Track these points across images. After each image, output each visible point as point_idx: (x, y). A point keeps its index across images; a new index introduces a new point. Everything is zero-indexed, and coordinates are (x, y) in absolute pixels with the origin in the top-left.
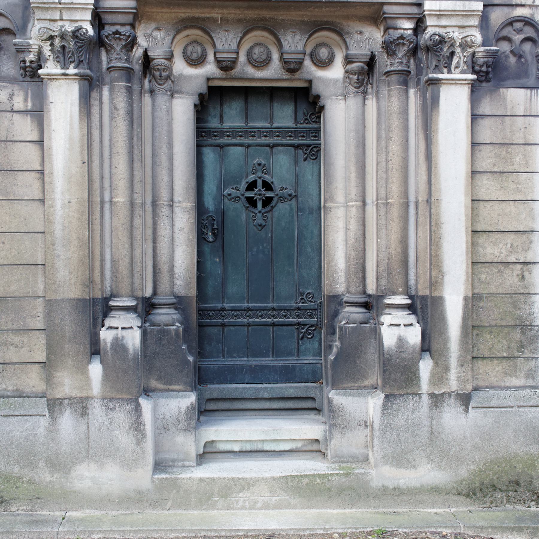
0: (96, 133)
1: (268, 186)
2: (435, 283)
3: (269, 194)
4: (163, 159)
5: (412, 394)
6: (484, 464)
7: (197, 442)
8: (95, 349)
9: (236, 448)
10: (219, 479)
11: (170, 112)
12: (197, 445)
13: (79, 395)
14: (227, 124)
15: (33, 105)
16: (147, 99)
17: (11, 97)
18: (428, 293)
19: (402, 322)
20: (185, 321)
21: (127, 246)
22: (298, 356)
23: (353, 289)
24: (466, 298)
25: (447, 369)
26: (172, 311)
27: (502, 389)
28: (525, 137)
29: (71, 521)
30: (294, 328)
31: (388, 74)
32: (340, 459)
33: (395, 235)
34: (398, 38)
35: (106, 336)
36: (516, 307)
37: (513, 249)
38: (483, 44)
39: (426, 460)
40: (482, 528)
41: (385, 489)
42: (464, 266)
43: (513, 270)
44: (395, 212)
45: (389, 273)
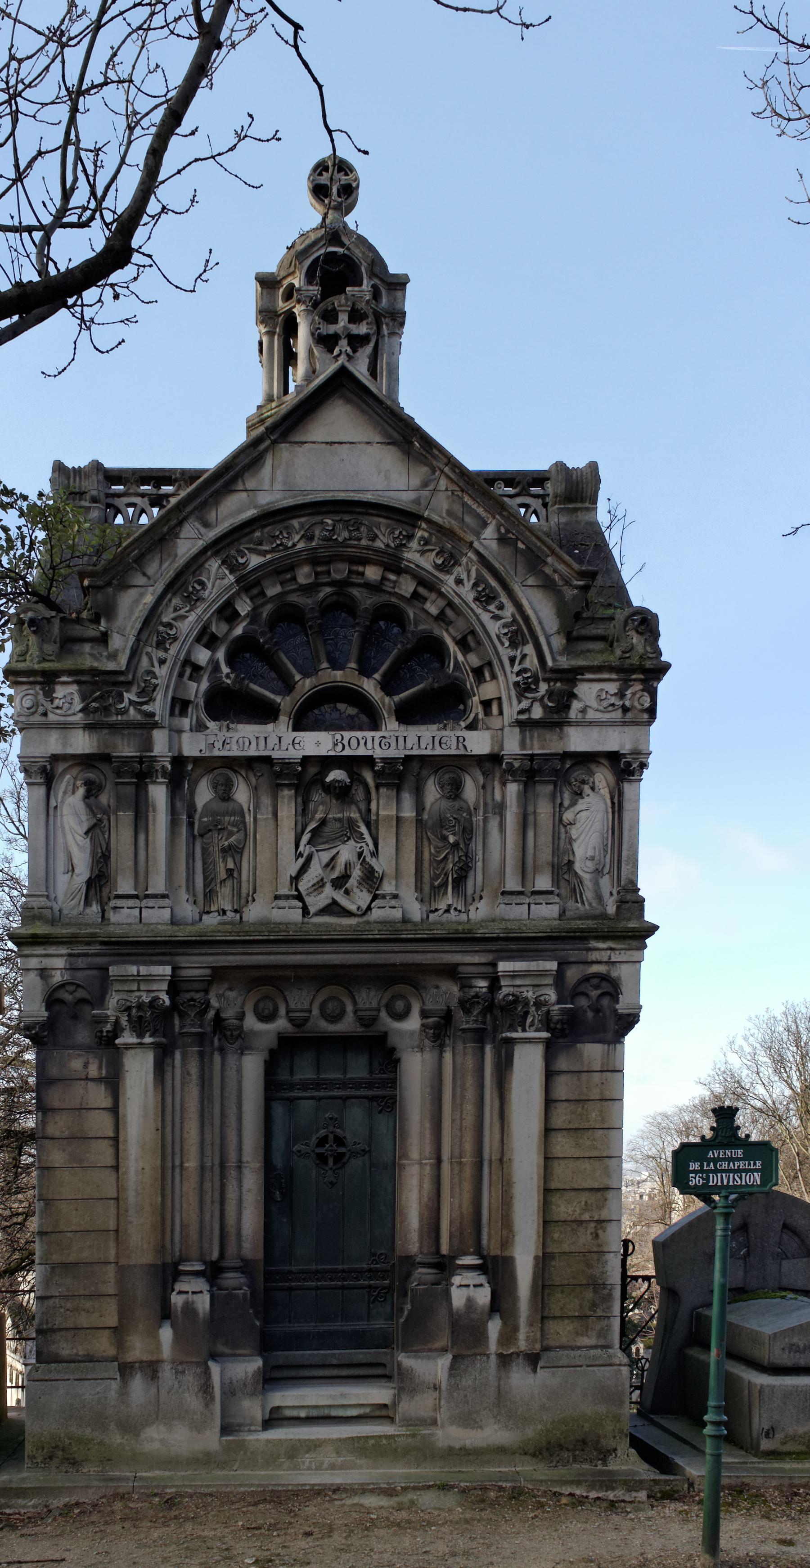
0: (169, 1099)
1: (340, 1141)
2: (507, 1242)
3: (342, 1150)
4: (232, 1120)
5: (480, 1354)
6: (552, 1423)
7: (263, 1407)
8: (166, 1313)
10: (286, 1440)
11: (239, 1070)
12: (263, 1410)
13: (150, 1358)
14: (297, 1077)
15: (107, 1072)
16: (217, 1058)
17: (86, 1065)
18: (499, 1253)
20: (252, 1286)
21: (197, 1210)
22: (368, 1320)
23: (425, 1250)
24: (536, 1258)
25: (516, 1329)
27: (573, 1348)
28: (602, 1094)
29: (141, 1478)
31: (464, 1031)
32: (408, 1422)
33: (467, 1197)
34: (473, 997)
35: (177, 1300)
36: (589, 1265)
37: (587, 1208)
39: (492, 1420)
40: (541, 1481)
41: (451, 1449)
42: (535, 1226)
43: (586, 1229)
44: (468, 1172)
45: (461, 1234)
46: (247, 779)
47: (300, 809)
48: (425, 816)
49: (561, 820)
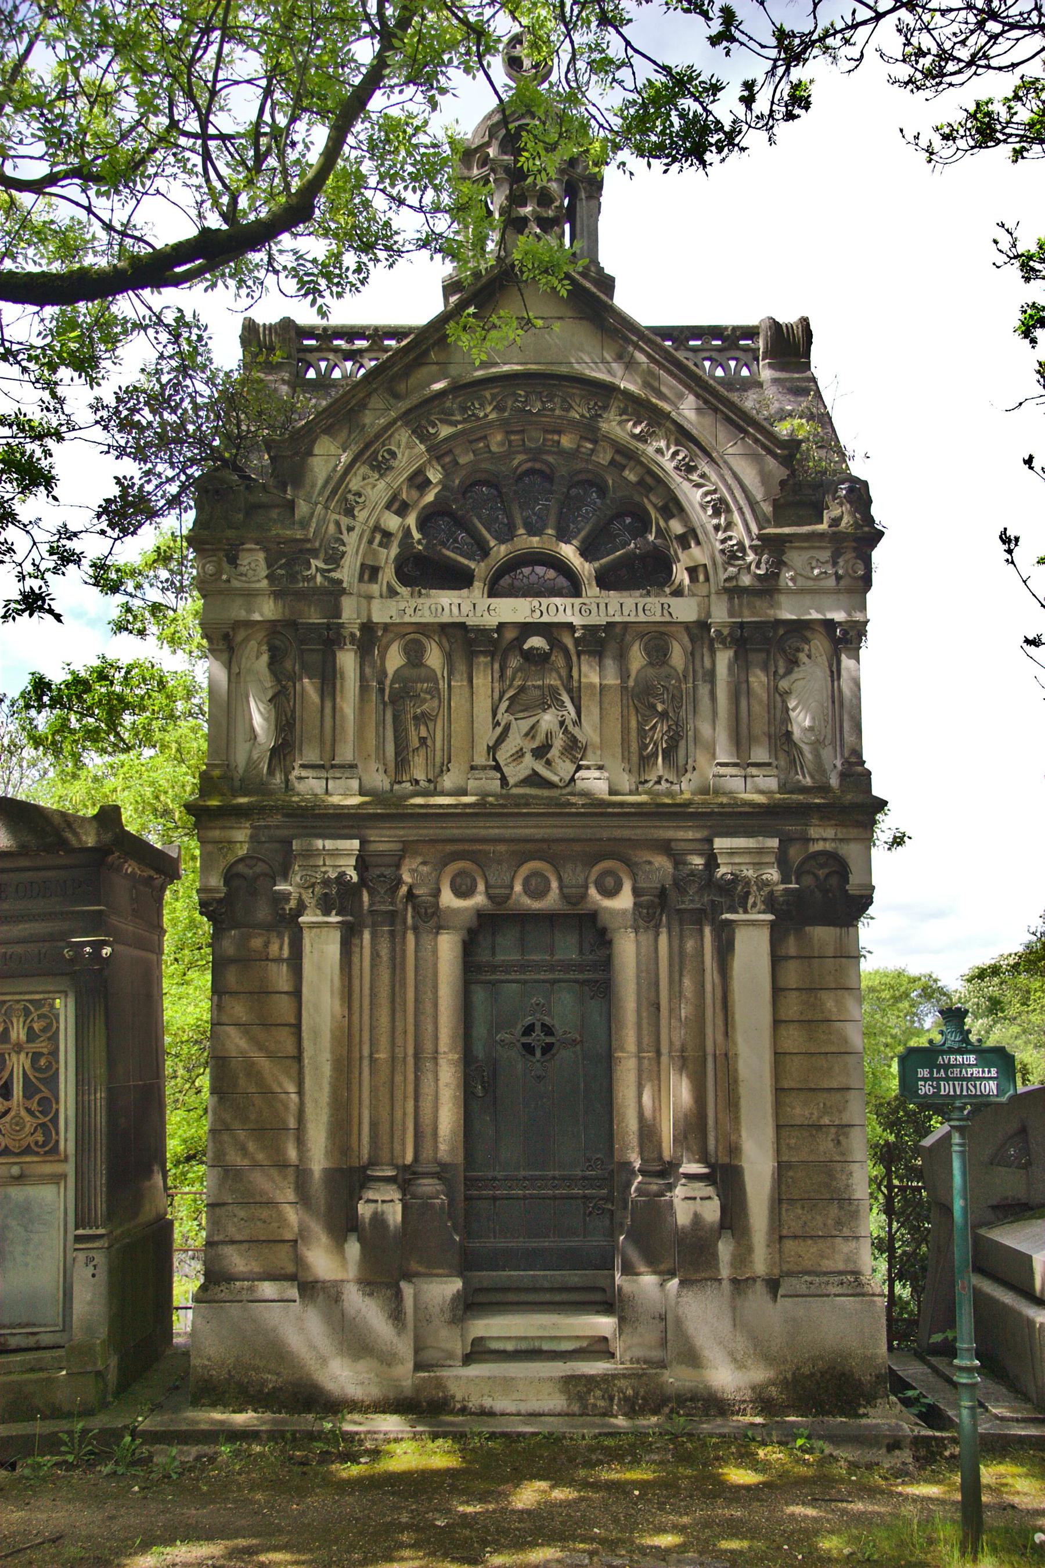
1: (548, 1030)
4: (428, 1008)
9: (510, 1347)
11: (435, 952)
14: (500, 958)
19: (698, 1194)
26: (436, 1181)
30: (579, 1202)
35: (364, 1210)
38: (783, 882)
46: (440, 645)
47: (497, 675)
48: (631, 683)
49: (776, 688)
